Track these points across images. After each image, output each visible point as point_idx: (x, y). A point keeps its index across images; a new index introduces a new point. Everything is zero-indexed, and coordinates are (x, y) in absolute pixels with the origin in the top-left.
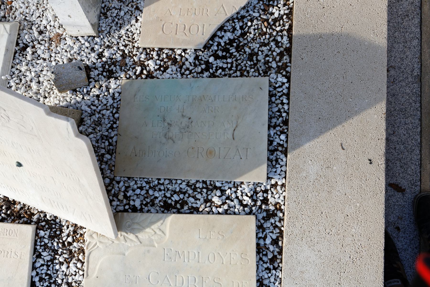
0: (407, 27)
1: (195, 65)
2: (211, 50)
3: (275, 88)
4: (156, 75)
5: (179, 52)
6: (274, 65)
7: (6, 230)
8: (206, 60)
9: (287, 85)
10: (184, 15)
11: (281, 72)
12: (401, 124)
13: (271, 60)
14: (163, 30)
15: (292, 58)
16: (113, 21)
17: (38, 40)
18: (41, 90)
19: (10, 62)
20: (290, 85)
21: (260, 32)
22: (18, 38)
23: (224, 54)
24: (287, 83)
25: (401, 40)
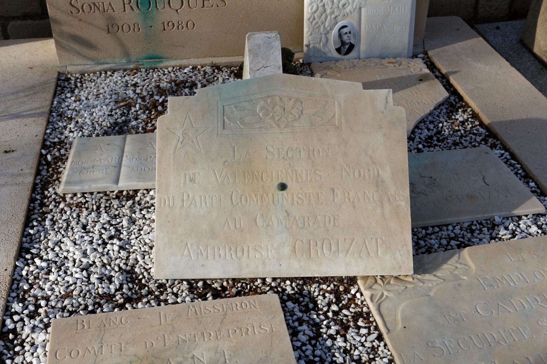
7: (234, 305)
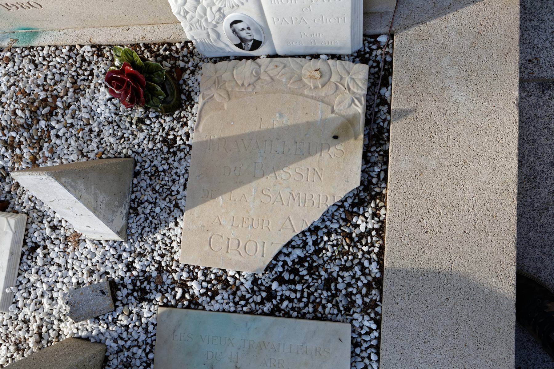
0: (546, 225)
1: (253, 292)
2: (274, 272)
3: (360, 335)
4: (202, 302)
5: (231, 273)
6: (359, 301)
8: (267, 285)
9: (376, 334)
10: (238, 226)
11: (369, 311)
12: (538, 362)
13: (355, 291)
14: (210, 245)
15: (384, 293)
16: (147, 219)
17: (51, 238)
18: (54, 310)
19: (15, 268)
20: (380, 334)
21: (340, 250)
22: (26, 235)
23: (292, 277)
24: (376, 330)
25: (538, 243)
